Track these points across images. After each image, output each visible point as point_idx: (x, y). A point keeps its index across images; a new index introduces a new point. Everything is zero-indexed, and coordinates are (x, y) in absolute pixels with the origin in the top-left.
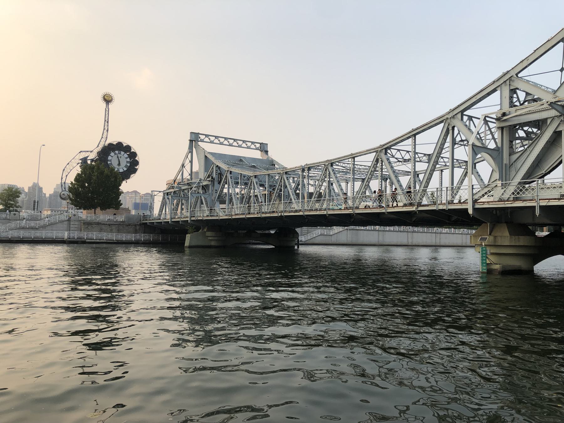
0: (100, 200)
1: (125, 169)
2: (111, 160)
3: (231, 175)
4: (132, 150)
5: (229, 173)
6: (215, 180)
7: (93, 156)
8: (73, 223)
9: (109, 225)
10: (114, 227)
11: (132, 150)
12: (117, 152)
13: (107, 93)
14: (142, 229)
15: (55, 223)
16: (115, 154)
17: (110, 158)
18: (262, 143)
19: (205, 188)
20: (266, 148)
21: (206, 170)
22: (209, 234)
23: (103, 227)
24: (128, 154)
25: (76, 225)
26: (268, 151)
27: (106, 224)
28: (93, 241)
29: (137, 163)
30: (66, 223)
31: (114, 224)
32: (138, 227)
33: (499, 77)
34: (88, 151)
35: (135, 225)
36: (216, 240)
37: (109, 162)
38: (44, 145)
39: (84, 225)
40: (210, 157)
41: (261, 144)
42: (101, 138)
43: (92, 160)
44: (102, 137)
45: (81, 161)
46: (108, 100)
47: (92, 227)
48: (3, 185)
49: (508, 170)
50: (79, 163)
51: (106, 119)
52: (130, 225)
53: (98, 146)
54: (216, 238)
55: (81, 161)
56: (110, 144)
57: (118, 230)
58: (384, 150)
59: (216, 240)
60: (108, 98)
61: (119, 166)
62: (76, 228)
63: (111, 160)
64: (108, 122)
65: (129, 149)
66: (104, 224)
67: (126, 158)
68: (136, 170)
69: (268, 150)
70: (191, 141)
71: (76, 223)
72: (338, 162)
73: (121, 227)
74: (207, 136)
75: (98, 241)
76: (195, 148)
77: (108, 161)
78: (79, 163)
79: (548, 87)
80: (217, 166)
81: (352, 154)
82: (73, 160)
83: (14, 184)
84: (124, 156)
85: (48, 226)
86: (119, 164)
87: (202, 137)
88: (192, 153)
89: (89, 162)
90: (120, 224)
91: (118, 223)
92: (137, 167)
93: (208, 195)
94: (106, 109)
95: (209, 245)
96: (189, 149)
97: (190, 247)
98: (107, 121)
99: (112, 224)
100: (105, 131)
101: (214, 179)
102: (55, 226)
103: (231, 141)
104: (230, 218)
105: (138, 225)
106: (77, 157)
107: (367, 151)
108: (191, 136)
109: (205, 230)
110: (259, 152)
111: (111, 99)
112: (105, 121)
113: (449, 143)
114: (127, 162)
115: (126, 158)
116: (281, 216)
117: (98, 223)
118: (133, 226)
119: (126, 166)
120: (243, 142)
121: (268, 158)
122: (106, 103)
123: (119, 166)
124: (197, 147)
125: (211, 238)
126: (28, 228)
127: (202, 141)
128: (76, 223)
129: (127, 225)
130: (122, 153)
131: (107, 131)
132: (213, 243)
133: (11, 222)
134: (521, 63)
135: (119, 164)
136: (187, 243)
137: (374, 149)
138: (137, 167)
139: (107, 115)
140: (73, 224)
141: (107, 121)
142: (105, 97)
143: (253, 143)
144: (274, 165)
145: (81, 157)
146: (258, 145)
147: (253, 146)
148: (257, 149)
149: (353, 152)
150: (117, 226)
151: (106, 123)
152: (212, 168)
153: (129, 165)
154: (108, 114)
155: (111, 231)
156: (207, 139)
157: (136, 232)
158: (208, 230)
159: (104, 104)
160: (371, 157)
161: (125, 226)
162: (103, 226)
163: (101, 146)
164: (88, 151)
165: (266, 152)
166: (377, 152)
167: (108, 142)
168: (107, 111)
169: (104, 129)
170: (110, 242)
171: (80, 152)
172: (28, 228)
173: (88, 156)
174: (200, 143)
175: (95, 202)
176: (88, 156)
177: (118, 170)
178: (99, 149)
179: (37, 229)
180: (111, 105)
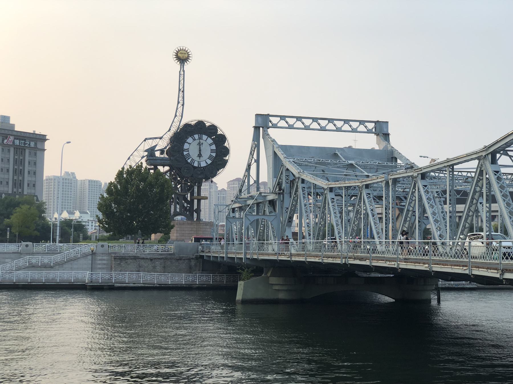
1: (209, 162)
2: (188, 150)
3: (303, 185)
4: (219, 132)
5: (300, 181)
6: (285, 191)
7: (163, 144)
8: (100, 258)
9: (151, 260)
10: (157, 263)
11: (219, 132)
12: (196, 136)
15: (76, 259)
17: (186, 146)
19: (272, 203)
20: (385, 130)
21: (275, 175)
23: (142, 262)
24: (212, 139)
25: (104, 260)
26: (388, 135)
27: (147, 259)
28: (125, 285)
29: (227, 151)
30: (90, 257)
31: (159, 259)
35: (190, 259)
36: (286, 290)
37: (185, 153)
38: (68, 143)
39: (114, 261)
40: (280, 153)
41: (376, 123)
43: (162, 151)
44: (176, 116)
45: (146, 153)
47: (126, 262)
51: (181, 87)
52: (181, 260)
53: (170, 129)
54: (285, 288)
55: (146, 153)
56: (187, 125)
58: (490, 156)
59: (286, 290)
60: (183, 55)
61: (200, 157)
62: (104, 264)
63: (188, 150)
64: (183, 92)
65: (213, 131)
66: (143, 259)
67: (211, 145)
69: (390, 132)
70: (257, 128)
71: (105, 258)
73: (168, 263)
74: (283, 118)
75: (132, 285)
77: (183, 150)
80: (287, 169)
81: (448, 161)
82: (135, 153)
83: (97, 180)
84: (207, 142)
85: (66, 262)
86: (200, 155)
87: (274, 120)
88: (258, 146)
89: (158, 154)
90: (166, 259)
92: (227, 158)
93: (274, 217)
94: (180, 72)
95: (276, 297)
96: (253, 140)
97: (244, 302)
98: (182, 91)
99: (155, 259)
100: (180, 105)
101: (283, 191)
103: (323, 123)
104: (289, 259)
105: (192, 259)
107: (468, 155)
108: (257, 121)
109: (269, 274)
110: (373, 137)
111: (186, 55)
112: (180, 90)
114: (212, 151)
115: (211, 145)
116: (345, 264)
117: (135, 257)
118: (186, 261)
119: (210, 157)
120: (344, 122)
122: (180, 63)
123: (200, 157)
124: (266, 135)
125: (277, 287)
126: (40, 267)
127: (275, 126)
128: (105, 258)
130: (205, 137)
131: (183, 105)
132: (281, 296)
135: (200, 155)
136: (239, 296)
137: (476, 153)
138: (227, 158)
140: (100, 260)
141: (182, 91)
142: (179, 55)
143: (362, 122)
144: (396, 159)
145: (147, 147)
146: (371, 126)
147: (362, 128)
148: (369, 131)
149: (451, 157)
150: (162, 261)
152: (282, 172)
153: (214, 155)
155: (154, 269)
156: (283, 123)
157: (190, 270)
158: (272, 275)
159: (177, 65)
160: (474, 164)
161: (174, 261)
163: (174, 130)
165: (386, 136)
166: (479, 158)
167: (183, 122)
168: (182, 75)
169: (178, 103)
170: (150, 287)
171: (145, 140)
172: (40, 267)
173: (157, 145)
175: (133, 225)
176: (156, 146)
177: (199, 163)
178: (171, 134)
179: (51, 267)
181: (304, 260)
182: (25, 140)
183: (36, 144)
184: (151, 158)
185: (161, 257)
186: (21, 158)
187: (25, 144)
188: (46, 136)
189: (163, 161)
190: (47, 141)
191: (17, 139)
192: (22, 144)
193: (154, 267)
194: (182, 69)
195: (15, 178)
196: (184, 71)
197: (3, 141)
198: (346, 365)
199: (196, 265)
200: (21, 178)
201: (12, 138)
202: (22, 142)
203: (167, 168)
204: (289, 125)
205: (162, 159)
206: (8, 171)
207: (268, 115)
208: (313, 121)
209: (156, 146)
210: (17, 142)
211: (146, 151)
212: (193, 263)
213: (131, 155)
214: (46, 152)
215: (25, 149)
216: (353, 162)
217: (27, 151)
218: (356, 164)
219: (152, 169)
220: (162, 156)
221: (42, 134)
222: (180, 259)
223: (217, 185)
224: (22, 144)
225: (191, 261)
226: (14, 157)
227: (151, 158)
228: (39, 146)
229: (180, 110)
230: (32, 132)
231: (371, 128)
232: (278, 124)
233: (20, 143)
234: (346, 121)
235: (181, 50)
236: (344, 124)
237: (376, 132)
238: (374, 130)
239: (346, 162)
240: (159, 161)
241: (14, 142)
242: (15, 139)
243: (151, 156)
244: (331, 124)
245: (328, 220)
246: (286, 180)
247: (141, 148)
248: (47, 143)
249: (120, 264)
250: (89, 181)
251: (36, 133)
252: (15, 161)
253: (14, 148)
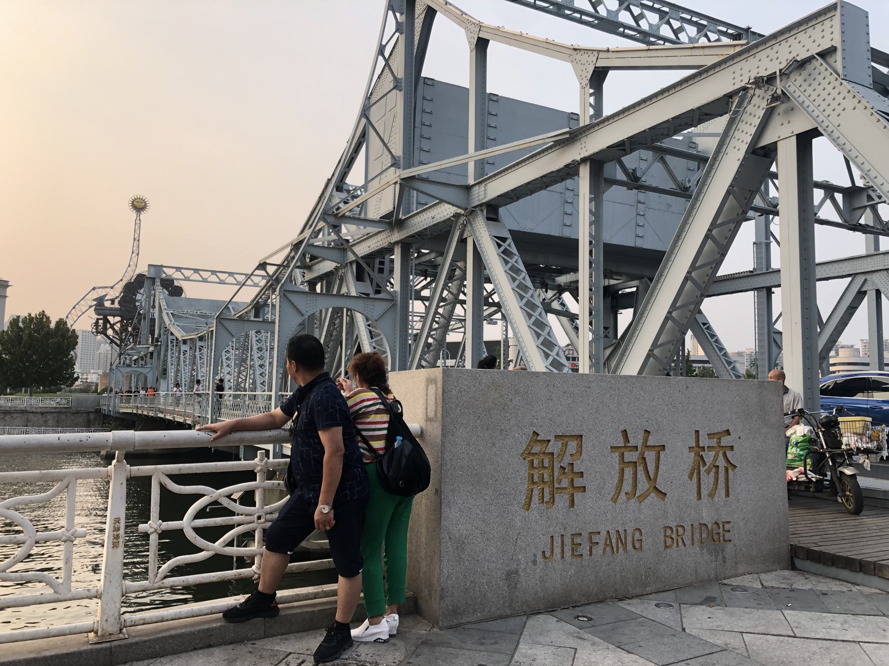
7: (116, 293)
9: (42, 413)
10: (50, 417)
13: (139, 197)
14: (100, 419)
23: (31, 416)
27: (37, 413)
32: (92, 416)
33: (353, 164)
34: (106, 287)
35: (88, 413)
37: (137, 304)
43: (113, 301)
46: (139, 206)
47: (12, 417)
49: (53, 532)
50: (91, 307)
52: (78, 413)
57: (58, 421)
60: (139, 204)
66: (33, 412)
78: (91, 307)
79: (139, 255)
82: (82, 302)
89: (107, 304)
90: (60, 412)
98: (137, 240)
99: (47, 412)
103: (223, 276)
105: (92, 412)
106: (90, 297)
111: (143, 204)
112: (135, 239)
113: (818, 260)
117: (23, 410)
118: (84, 415)
129: (74, 414)
131: (138, 254)
134: (646, 52)
141: (137, 240)
142: (135, 203)
150: (55, 414)
159: (133, 214)
162: (32, 414)
164: (106, 287)
167: (137, 272)
168: (138, 223)
173: (107, 295)
176: (106, 295)
180: (143, 215)
181: (131, 411)
184: (99, 308)
185: (55, 410)
188: (8, 282)
189: (112, 311)
190: (9, 287)
193: (46, 422)
194: (138, 218)
196: (140, 220)
198: (336, 505)
199: (95, 419)
203: (118, 319)
205: (111, 309)
207: (162, 266)
208: (176, 271)
209: (106, 295)
211: (94, 300)
212: (92, 416)
213: (77, 304)
214: (7, 299)
219: (101, 319)
220: (113, 306)
222: (78, 413)
223: (855, 347)
225: (89, 415)
227: (99, 308)
229: (134, 259)
235: (137, 198)
240: (107, 311)
243: (99, 306)
247: (90, 297)
248: (9, 289)
249: (3, 418)
250: (83, 332)
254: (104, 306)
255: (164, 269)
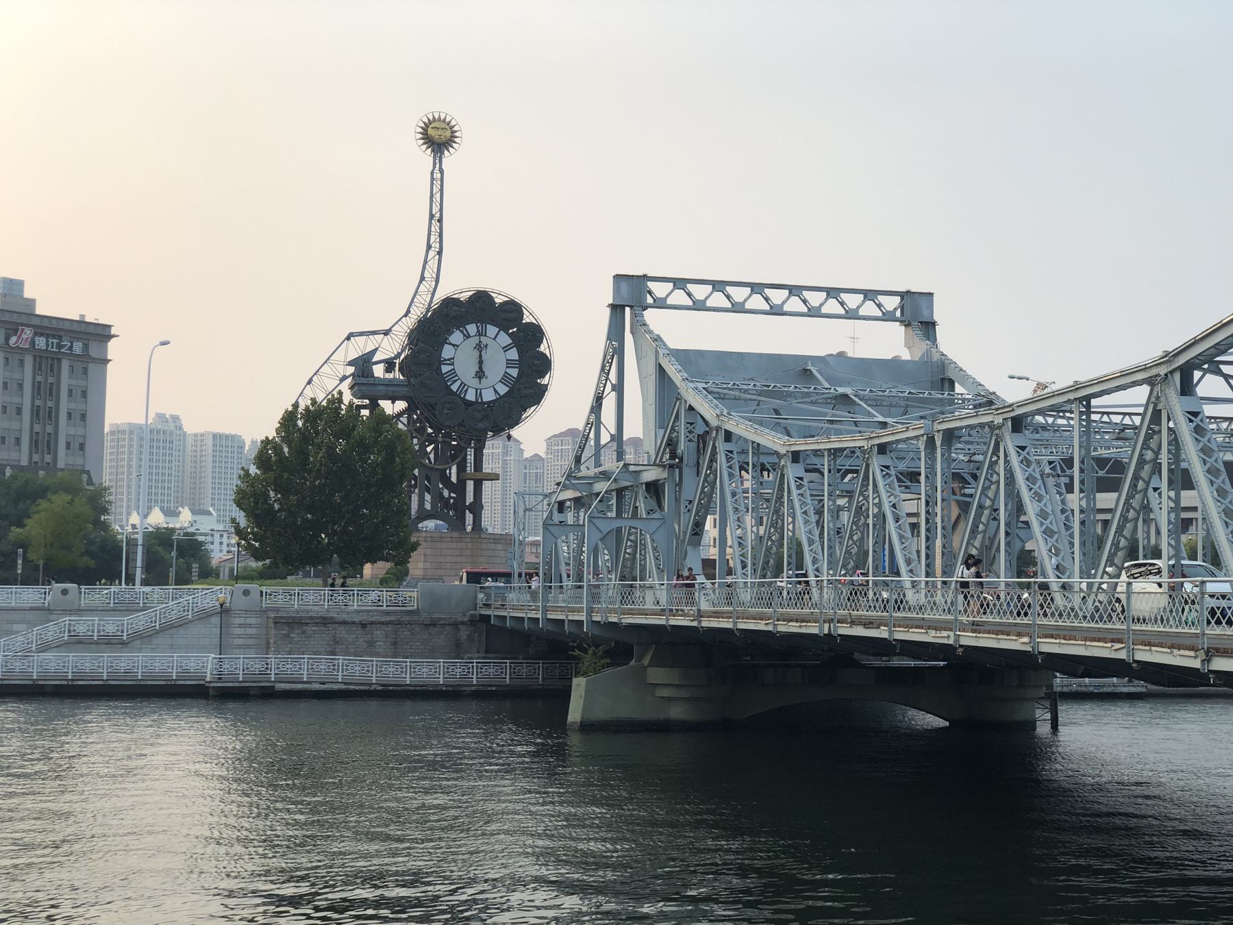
0: (335, 533)
1: (503, 390)
2: (451, 361)
3: (729, 446)
4: (527, 319)
5: (721, 436)
6: (685, 461)
7: (392, 347)
8: (241, 621)
9: (364, 625)
10: (378, 633)
11: (527, 319)
12: (472, 329)
15: (182, 624)
16: (467, 336)
17: (447, 352)
18: (908, 292)
19: (654, 489)
20: (925, 312)
21: (661, 423)
22: (656, 675)
23: (342, 632)
24: (510, 335)
25: (250, 626)
26: (934, 324)
27: (353, 623)
28: (300, 686)
29: (545, 365)
30: (216, 620)
31: (382, 623)
35: (456, 625)
36: (688, 699)
37: (445, 369)
38: (163, 344)
39: (275, 628)
41: (905, 295)
42: (421, 282)
43: (389, 365)
44: (422, 278)
45: (351, 370)
47: (303, 632)
48: (199, 438)
51: (435, 209)
52: (435, 625)
53: (408, 312)
54: (684, 693)
55: (351, 370)
56: (449, 302)
58: (1177, 376)
59: (688, 699)
61: (480, 378)
62: (250, 636)
63: (451, 361)
64: (440, 221)
65: (513, 315)
66: (344, 623)
67: (506, 349)
68: (543, 390)
69: (936, 317)
70: (617, 309)
71: (253, 621)
72: (1040, 412)
75: (317, 686)
76: (632, 332)
77: (441, 362)
81: (1077, 387)
82: (325, 369)
84: (498, 343)
86: (480, 374)
87: (660, 289)
88: (619, 352)
89: (379, 371)
90: (399, 623)
91: (392, 618)
92: (545, 381)
93: (658, 523)
94: (432, 173)
96: (609, 338)
97: (587, 727)
98: (436, 218)
99: (373, 623)
100: (432, 253)
101: (681, 460)
102: (181, 631)
104: (695, 624)
105: (462, 623)
107: (1124, 374)
108: (617, 291)
110: (897, 330)
111: (448, 134)
112: (432, 216)
114: (510, 363)
115: (506, 349)
116: (829, 635)
117: (325, 618)
118: (448, 628)
119: (505, 379)
120: (828, 295)
121: (928, 353)
123: (480, 378)
125: (665, 693)
126: (96, 643)
127: (661, 304)
128: (253, 621)
130: (492, 330)
131: (440, 253)
132: (676, 712)
133: (53, 617)
135: (480, 374)
136: (575, 714)
137: (1145, 368)
138: (545, 381)
139: (438, 195)
140: (240, 626)
141: (436, 218)
142: (430, 131)
143: (869, 295)
144: (952, 383)
145: (353, 355)
146: (891, 303)
148: (887, 317)
149: (1083, 377)
150: (389, 628)
151: (435, 224)
152: (677, 414)
153: (514, 372)
154: (442, 190)
155: (370, 648)
156: (679, 297)
157: (457, 651)
158: (654, 663)
159: (425, 157)
163: (417, 312)
165: (928, 327)
166: (1150, 381)
167: (441, 295)
168: (437, 180)
169: (429, 247)
171: (348, 338)
172: (96, 643)
173: (376, 349)
174: (650, 316)
176: (374, 352)
177: (479, 393)
178: (410, 322)
179: (123, 643)
181: (730, 626)
182: (60, 338)
183: (86, 347)
184: (364, 380)
185: (388, 619)
186: (51, 380)
187: (60, 346)
188: (110, 327)
189: (390, 388)
190: (113, 340)
191: (42, 335)
192: (52, 347)
193: (371, 644)
195: (37, 428)
197: (7, 339)
200: (49, 429)
201: (28, 333)
202: (52, 343)
203: (401, 405)
204: (733, 305)
206: (19, 411)
207: (645, 278)
209: (374, 352)
210: (41, 342)
211: (350, 363)
213: (315, 374)
214: (109, 366)
215: (59, 360)
216: (848, 390)
217: (65, 364)
218: (856, 396)
219: (364, 407)
220: (390, 376)
221: (101, 322)
222: (433, 624)
223: (522, 447)
224: (52, 347)
225: (458, 629)
226: (34, 378)
227: (364, 380)
228: (93, 352)
229: (432, 264)
230: (77, 318)
231: (855, 307)
232: (668, 299)
233: (47, 345)
234: (832, 292)
235: (434, 120)
236: (826, 299)
237: (903, 319)
238: (898, 314)
239: (832, 391)
240: (382, 388)
241: (33, 343)
242: (36, 334)
243: (363, 376)
244: (795, 299)
245: (788, 530)
246: (688, 434)
247: (340, 356)
248: (112, 344)
249: (287, 636)
250: (215, 436)
251: (87, 319)
252: (37, 389)
253: (35, 357)
254: (372, 375)
255: (649, 284)
